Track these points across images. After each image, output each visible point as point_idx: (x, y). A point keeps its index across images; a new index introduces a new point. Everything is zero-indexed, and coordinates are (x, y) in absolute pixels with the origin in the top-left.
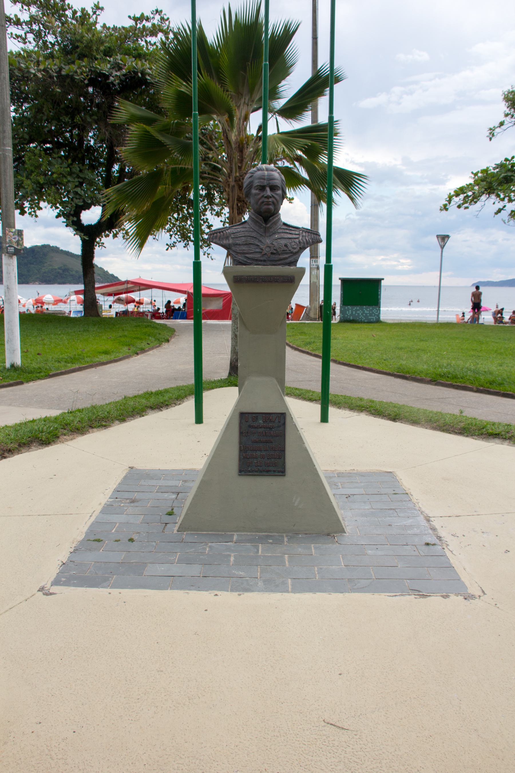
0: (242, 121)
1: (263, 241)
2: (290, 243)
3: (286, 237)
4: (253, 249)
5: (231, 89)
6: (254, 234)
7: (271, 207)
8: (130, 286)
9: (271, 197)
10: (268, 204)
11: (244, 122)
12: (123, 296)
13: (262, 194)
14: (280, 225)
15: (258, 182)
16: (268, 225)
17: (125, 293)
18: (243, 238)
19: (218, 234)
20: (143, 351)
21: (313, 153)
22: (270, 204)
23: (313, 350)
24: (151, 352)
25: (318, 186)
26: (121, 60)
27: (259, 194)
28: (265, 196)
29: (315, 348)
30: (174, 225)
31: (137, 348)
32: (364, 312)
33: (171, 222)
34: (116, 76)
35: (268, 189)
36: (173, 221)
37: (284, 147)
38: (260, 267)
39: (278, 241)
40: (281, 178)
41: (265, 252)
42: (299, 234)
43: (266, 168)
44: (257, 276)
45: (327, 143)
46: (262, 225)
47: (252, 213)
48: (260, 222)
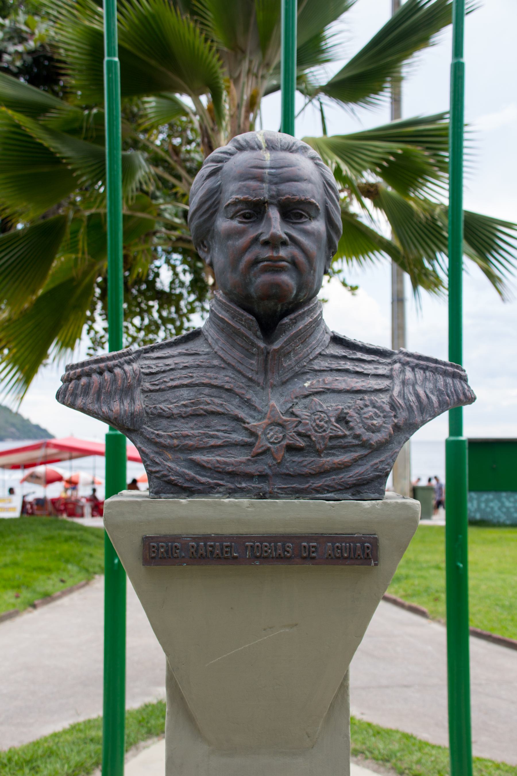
0: (243, 110)
1: (256, 401)
2: (359, 410)
3: (342, 386)
4: (220, 432)
5: (218, 36)
6: (223, 378)
7: (287, 279)
8: (52, 451)
9: (284, 243)
10: (274, 267)
11: (248, 112)
12: (41, 470)
13: (252, 234)
14: (319, 342)
15: (239, 191)
16: (276, 346)
17: (42, 463)
18: (184, 392)
19: (95, 377)
20: (48, 598)
21: (404, 173)
22: (281, 270)
23: (407, 596)
24: (65, 601)
25: (414, 251)
26: (26, 24)
27: (240, 233)
28: (264, 238)
29: (410, 592)
30: (134, 339)
31: (34, 591)
32: (503, 504)
33: (127, 333)
34: (17, 52)
35: (274, 214)
36: (132, 331)
37: (339, 161)
38: (245, 501)
39: (309, 401)
40: (322, 175)
41: (263, 443)
42: (389, 377)
43: (267, 141)
44: (230, 537)
45: (446, 143)
46: (253, 345)
47: (218, 301)
48: (248, 333)
